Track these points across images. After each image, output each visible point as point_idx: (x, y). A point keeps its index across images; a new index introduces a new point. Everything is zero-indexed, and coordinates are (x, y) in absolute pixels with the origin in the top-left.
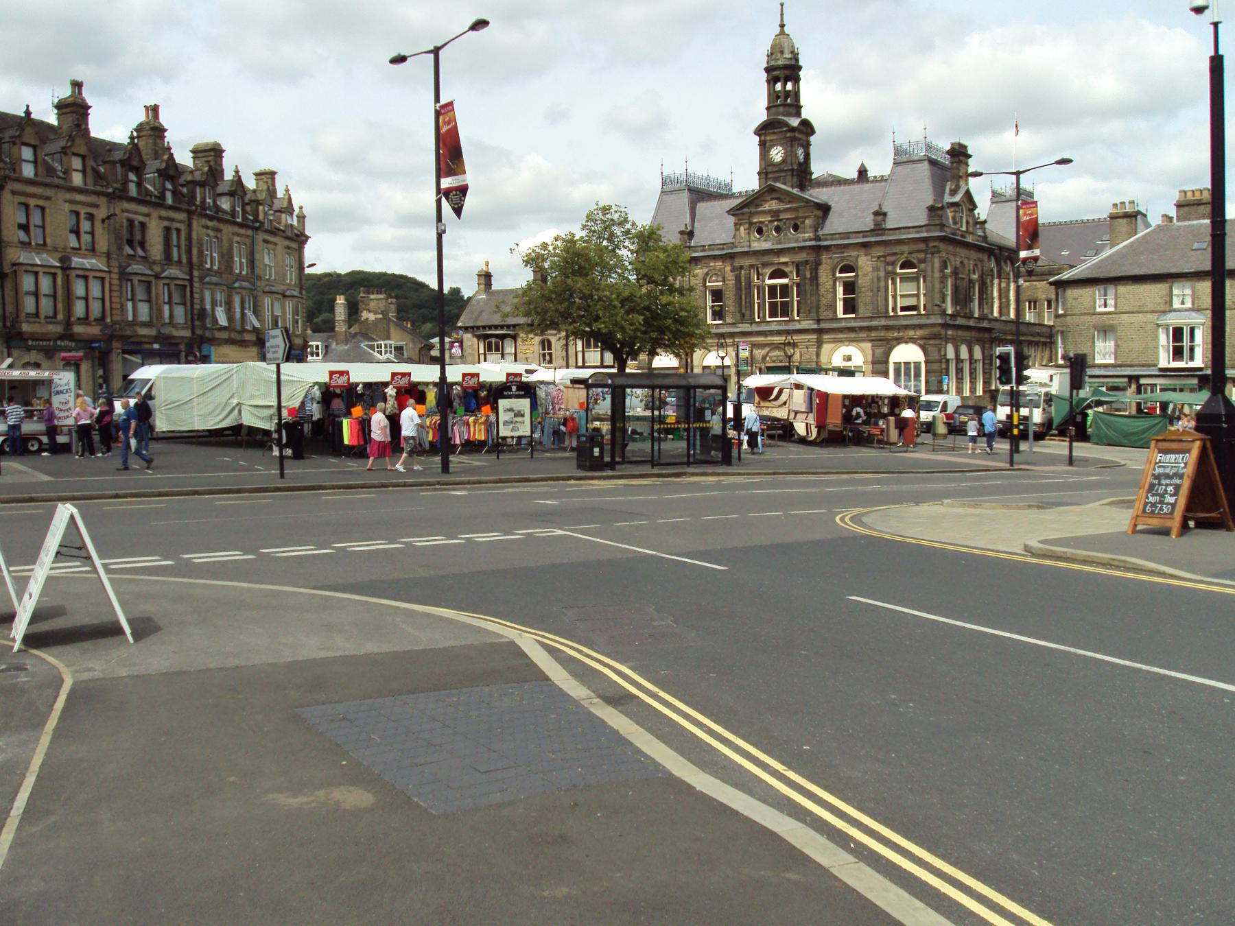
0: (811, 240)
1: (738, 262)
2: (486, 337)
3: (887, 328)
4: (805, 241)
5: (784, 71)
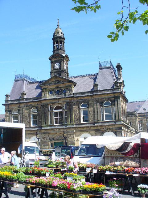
5: (58, 40)
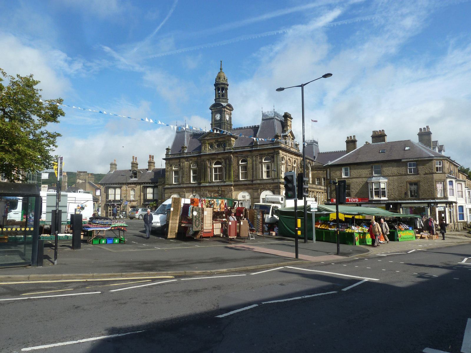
4: (227, 150)
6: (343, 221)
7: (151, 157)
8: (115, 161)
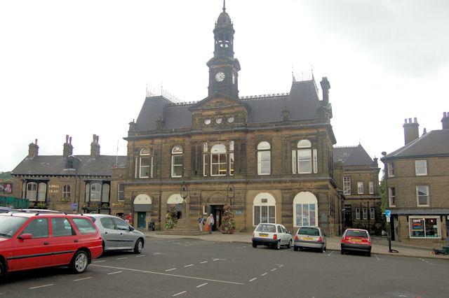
0: (243, 126)
1: (193, 138)
2: (29, 181)
3: (292, 182)
4: (238, 127)
5: (224, 30)
6: (237, 95)
7: (96, 138)
8: (36, 140)
